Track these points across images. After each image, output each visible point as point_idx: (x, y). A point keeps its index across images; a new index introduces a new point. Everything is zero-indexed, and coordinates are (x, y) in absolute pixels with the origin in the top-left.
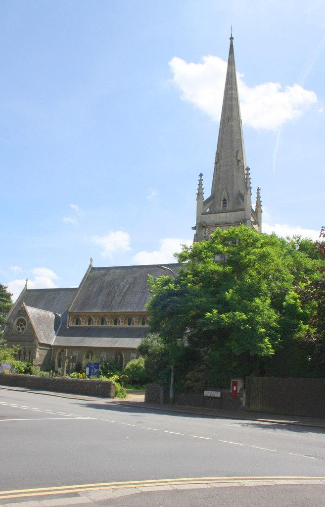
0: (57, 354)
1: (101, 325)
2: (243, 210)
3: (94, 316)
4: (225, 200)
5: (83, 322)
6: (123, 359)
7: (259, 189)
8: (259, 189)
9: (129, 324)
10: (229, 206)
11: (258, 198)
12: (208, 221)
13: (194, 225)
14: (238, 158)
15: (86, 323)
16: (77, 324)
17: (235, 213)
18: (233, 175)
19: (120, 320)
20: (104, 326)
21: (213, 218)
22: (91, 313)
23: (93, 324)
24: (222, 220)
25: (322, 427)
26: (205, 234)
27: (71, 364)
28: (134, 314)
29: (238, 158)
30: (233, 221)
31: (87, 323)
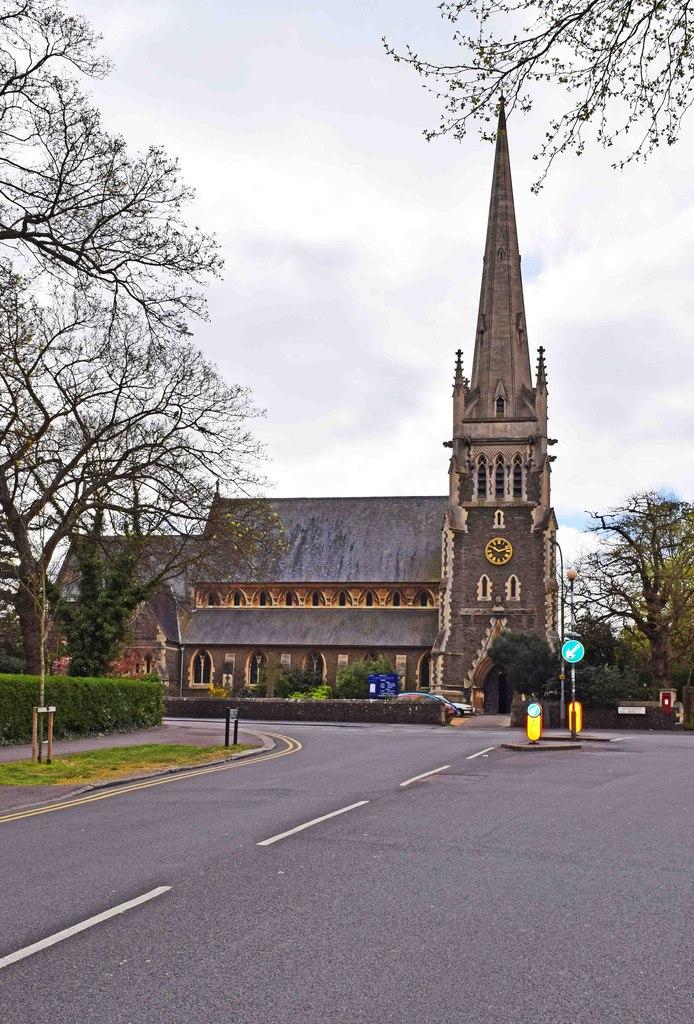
0: (193, 659)
1: (314, 604)
2: (533, 420)
3: (245, 589)
4: (500, 400)
5: (224, 600)
6: (322, 664)
7: (541, 350)
8: (541, 350)
9: (342, 603)
10: (508, 411)
11: (541, 367)
12: (474, 435)
13: (449, 438)
14: (521, 327)
15: (229, 601)
16: (262, 603)
17: (522, 423)
18: (512, 358)
19: (325, 597)
20: (293, 606)
21: (480, 430)
22: (337, 583)
23: (244, 604)
24: (498, 435)
25: (691, 730)
26: (469, 456)
27: (225, 675)
28: (325, 586)
29: (521, 327)
30: (611, 526)
31: (233, 602)
